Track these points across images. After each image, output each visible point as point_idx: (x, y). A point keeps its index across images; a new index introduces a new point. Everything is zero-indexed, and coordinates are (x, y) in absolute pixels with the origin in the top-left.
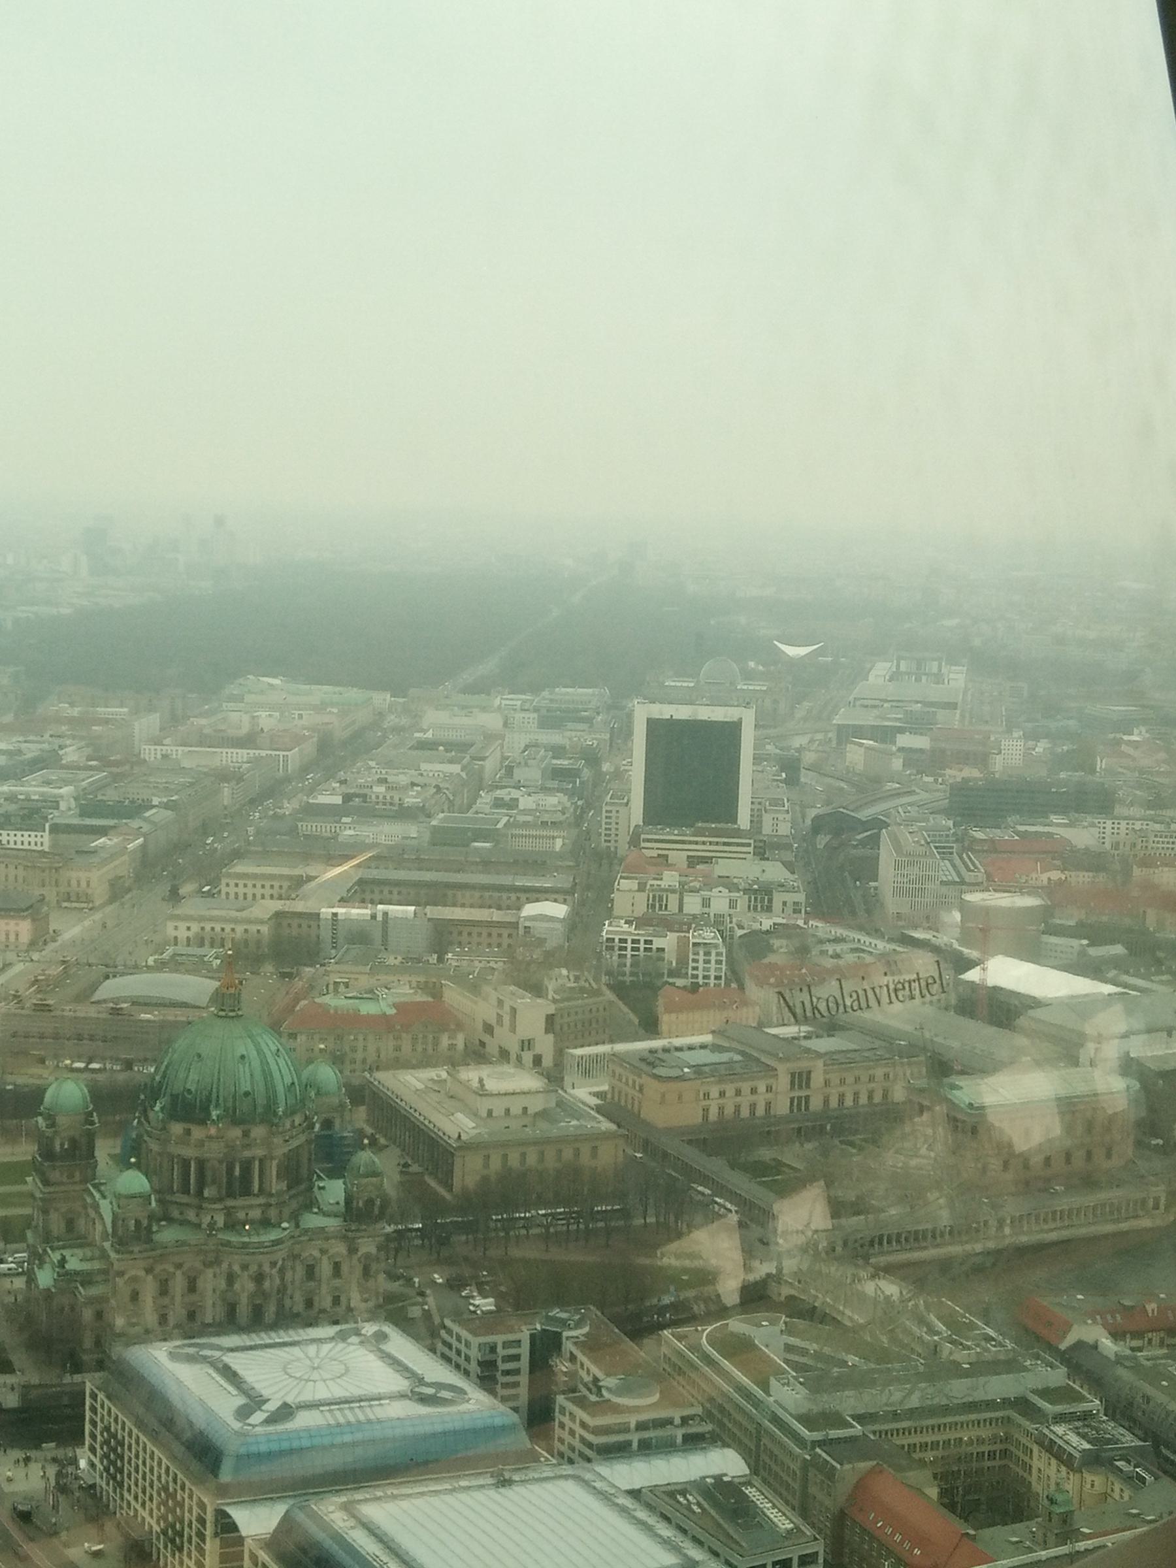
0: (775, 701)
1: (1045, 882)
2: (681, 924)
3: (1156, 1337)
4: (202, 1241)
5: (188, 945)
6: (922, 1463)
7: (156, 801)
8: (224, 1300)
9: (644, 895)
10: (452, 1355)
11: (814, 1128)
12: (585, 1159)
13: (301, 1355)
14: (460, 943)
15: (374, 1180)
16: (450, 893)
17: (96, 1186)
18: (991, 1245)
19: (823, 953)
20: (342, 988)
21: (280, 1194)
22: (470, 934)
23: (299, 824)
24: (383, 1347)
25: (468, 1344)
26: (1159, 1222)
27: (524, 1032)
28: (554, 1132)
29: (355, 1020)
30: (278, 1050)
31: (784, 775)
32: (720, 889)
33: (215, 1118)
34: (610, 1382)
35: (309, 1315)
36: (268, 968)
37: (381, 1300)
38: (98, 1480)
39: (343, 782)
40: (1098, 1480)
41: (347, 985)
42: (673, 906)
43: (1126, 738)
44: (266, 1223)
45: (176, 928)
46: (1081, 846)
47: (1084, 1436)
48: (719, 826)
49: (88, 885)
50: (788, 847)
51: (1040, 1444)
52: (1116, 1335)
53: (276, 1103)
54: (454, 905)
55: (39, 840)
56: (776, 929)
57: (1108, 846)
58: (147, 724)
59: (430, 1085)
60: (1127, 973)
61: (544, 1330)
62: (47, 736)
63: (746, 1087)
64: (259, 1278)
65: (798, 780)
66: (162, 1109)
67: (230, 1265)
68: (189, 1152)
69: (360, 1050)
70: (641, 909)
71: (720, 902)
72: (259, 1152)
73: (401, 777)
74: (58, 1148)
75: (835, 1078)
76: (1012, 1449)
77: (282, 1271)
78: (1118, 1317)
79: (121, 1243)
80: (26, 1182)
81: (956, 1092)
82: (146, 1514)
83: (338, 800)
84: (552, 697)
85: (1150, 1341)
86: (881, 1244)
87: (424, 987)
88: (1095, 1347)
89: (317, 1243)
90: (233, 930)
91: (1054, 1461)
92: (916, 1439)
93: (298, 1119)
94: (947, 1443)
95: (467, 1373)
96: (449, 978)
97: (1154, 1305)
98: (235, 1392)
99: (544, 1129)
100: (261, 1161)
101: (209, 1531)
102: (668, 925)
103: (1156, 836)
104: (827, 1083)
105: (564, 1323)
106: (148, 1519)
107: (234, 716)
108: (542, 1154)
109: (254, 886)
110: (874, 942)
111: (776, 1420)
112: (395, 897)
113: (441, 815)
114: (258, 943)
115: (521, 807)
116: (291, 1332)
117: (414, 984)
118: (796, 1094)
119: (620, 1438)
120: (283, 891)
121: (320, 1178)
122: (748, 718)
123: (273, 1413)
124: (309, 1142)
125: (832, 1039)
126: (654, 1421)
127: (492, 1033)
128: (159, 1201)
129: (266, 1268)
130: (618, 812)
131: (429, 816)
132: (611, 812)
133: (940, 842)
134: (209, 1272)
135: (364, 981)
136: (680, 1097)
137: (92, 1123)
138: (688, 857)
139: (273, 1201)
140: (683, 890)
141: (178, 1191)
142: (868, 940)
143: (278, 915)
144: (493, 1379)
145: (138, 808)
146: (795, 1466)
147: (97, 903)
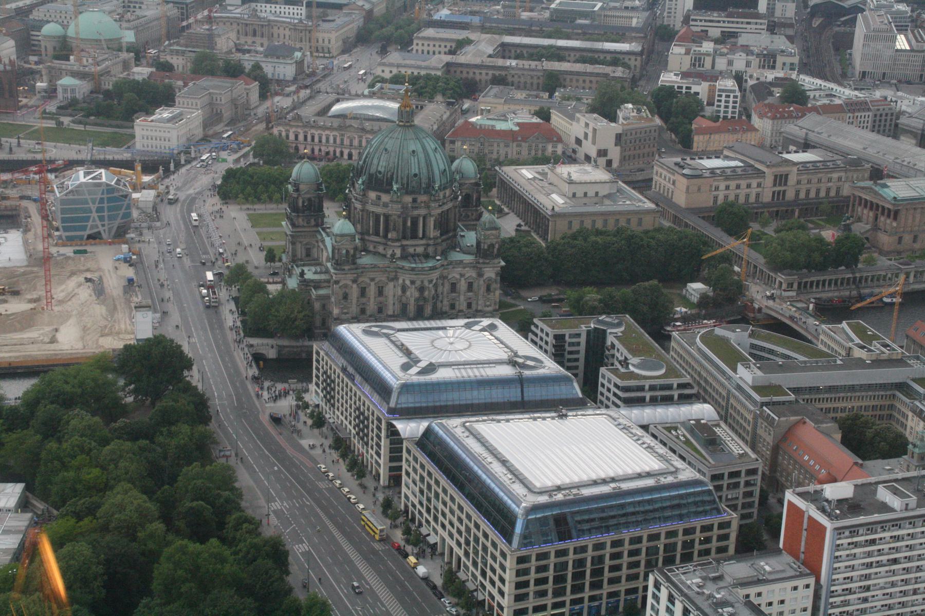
2: (712, 77)
10: (538, 340)
11: (787, 211)
12: (634, 226)
15: (494, 232)
17: (324, 229)
21: (435, 238)
25: (547, 335)
29: (492, 133)
34: (634, 360)
38: (321, 403)
41: (489, 111)
44: (427, 256)
50: (791, 26)
51: (914, 412)
53: (434, 182)
59: (537, 176)
61: (595, 328)
63: (743, 183)
64: (421, 289)
66: (363, 183)
67: (404, 280)
68: (379, 210)
69: (495, 153)
70: (686, 66)
71: (739, 62)
72: (423, 212)
74: (300, 204)
75: (804, 178)
77: (436, 286)
79: (338, 264)
80: (281, 226)
81: (885, 190)
82: (347, 423)
93: (448, 192)
95: (546, 351)
100: (424, 218)
101: (383, 435)
102: (703, 77)
104: (799, 182)
106: (349, 426)
108: (606, 221)
111: (739, 388)
118: (777, 189)
119: (639, 394)
121: (463, 231)
123: (423, 369)
125: (805, 154)
128: (362, 239)
129: (426, 283)
134: (391, 285)
136: (699, 189)
137: (322, 190)
139: (431, 242)
142: (839, 88)
143: (448, 65)
144: (562, 355)
146: (750, 417)
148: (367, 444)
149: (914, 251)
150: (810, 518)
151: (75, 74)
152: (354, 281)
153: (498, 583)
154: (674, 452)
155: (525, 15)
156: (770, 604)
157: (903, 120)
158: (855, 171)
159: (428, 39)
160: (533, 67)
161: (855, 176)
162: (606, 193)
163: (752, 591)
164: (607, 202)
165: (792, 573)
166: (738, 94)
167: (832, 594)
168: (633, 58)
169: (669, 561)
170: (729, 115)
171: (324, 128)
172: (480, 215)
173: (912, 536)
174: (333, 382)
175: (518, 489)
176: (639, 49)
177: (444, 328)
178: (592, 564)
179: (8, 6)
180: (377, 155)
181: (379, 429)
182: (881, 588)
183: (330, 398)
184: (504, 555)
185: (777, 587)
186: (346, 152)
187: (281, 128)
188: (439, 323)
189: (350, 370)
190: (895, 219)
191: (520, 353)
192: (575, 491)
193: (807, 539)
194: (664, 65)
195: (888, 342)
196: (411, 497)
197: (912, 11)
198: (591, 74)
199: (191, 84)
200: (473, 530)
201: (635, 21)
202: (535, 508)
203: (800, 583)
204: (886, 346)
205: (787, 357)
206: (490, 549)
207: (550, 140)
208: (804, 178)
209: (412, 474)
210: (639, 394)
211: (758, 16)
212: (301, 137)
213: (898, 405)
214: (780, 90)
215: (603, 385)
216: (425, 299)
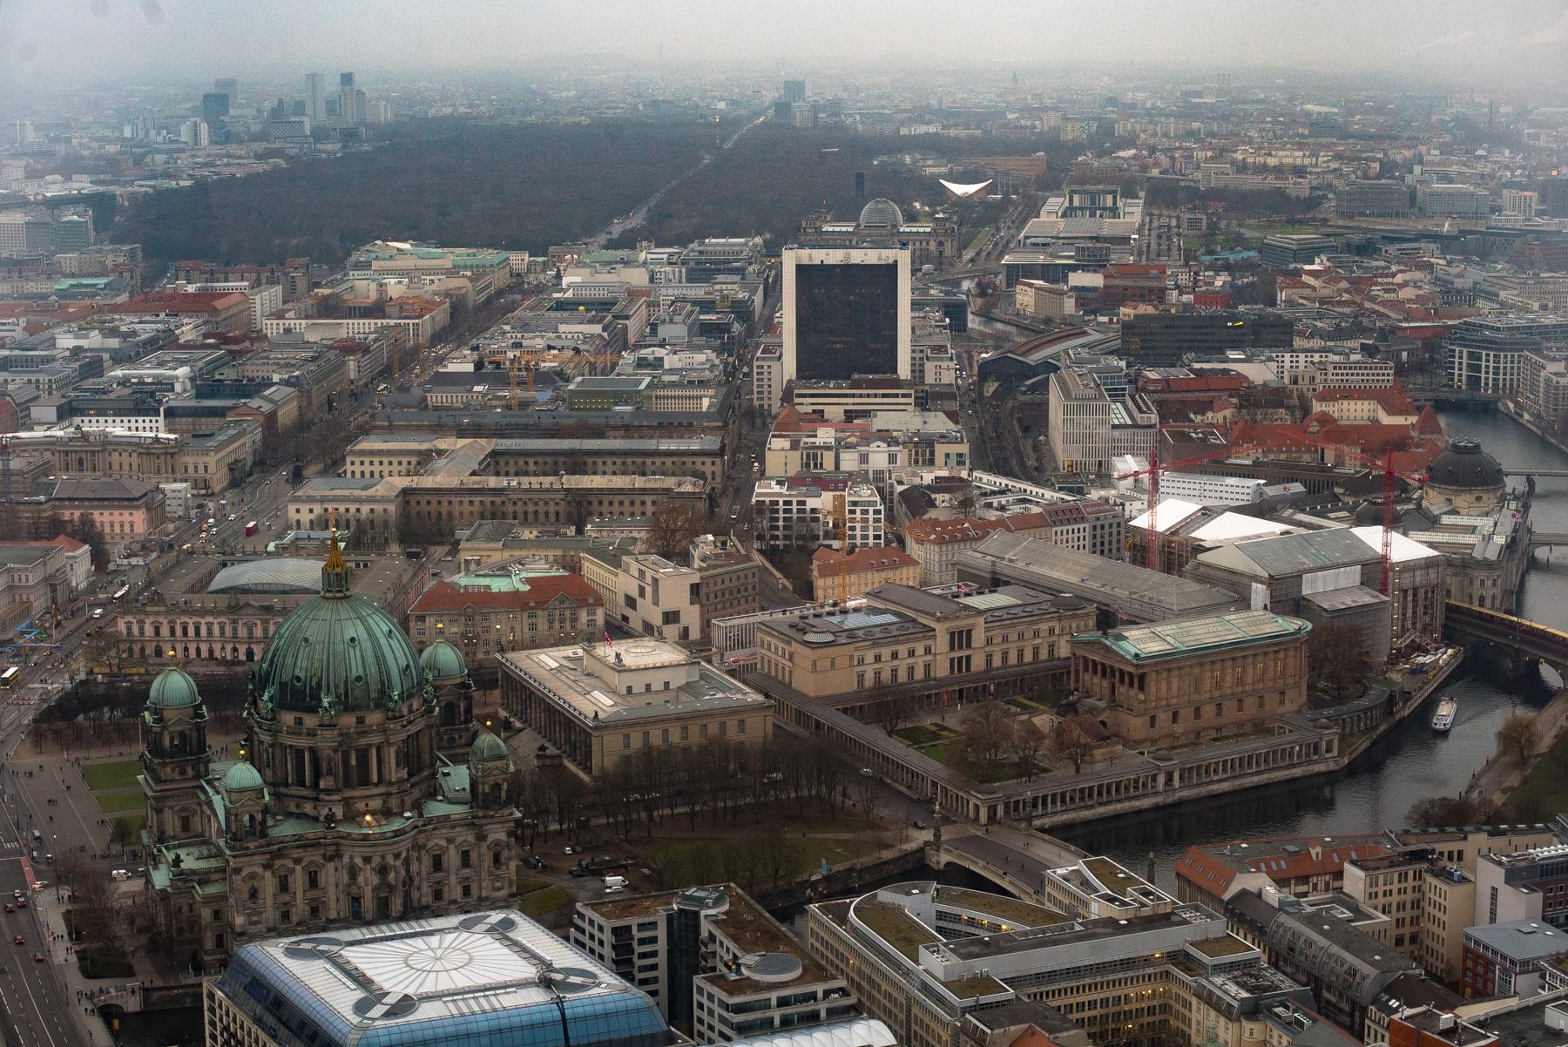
0: (941, 244)
1: (1221, 421)
2: (836, 482)
3: (1321, 881)
4: (321, 834)
5: (312, 528)
6: (1080, 1023)
7: (276, 378)
8: (349, 894)
9: (798, 453)
10: (586, 940)
11: (976, 689)
12: (733, 734)
13: (424, 946)
14: (601, 514)
15: (499, 763)
16: (590, 460)
17: (209, 782)
18: (1160, 799)
19: (990, 505)
20: (473, 567)
21: (400, 782)
22: (611, 503)
23: (429, 395)
24: (511, 935)
25: (601, 928)
26: (1332, 766)
27: (668, 604)
29: (488, 600)
30: (390, 631)
31: (948, 320)
32: (879, 443)
33: (326, 704)
34: (749, 959)
36: (395, 548)
37: (514, 889)
39: (475, 348)
40: (1256, 1027)
41: (478, 563)
43: (1307, 267)
44: (386, 813)
45: (298, 511)
48: (877, 377)
49: (206, 471)
50: (952, 396)
51: (1199, 997)
52: (1281, 882)
53: (391, 688)
54: (595, 473)
55: (154, 425)
56: (941, 485)
57: (1286, 380)
58: (267, 298)
59: (565, 663)
60: (1303, 511)
62: (162, 315)
63: (903, 650)
64: (383, 870)
65: (966, 324)
66: (271, 699)
67: (351, 858)
68: (302, 742)
70: (794, 467)
71: (879, 457)
72: (375, 739)
73: (538, 340)
74: (167, 743)
75: (997, 635)
76: (1173, 1003)
77: (407, 863)
78: (1283, 863)
83: (470, 368)
84: (701, 248)
85: (1315, 886)
86: (1044, 804)
88: (1259, 895)
89: (445, 831)
90: (358, 510)
91: (1213, 1013)
92: (1073, 1000)
94: (1105, 1002)
95: (601, 957)
97: (1319, 849)
98: (353, 987)
99: (687, 704)
100: (379, 749)
103: (1335, 368)
104: (989, 641)
105: (700, 902)
107: (361, 285)
109: (381, 463)
110: (1041, 491)
111: (925, 988)
112: (532, 467)
113: (579, 379)
114: (386, 522)
115: (667, 366)
116: (423, 922)
117: (551, 559)
118: (957, 654)
120: (412, 467)
122: (904, 259)
123: (393, 1006)
124: (430, 727)
126: (796, 996)
127: (634, 608)
129: (390, 860)
130: (769, 367)
131: (568, 380)
132: (762, 367)
133: (1112, 384)
134: (331, 866)
135: (497, 557)
137: (202, 716)
138: (846, 411)
139: (394, 789)
140: (840, 446)
141: (293, 784)
142: (1035, 490)
143: (405, 492)
144: (630, 962)
145: (256, 387)
147: (217, 490)
149: (1173, 736)
152: (266, 867)
158: (1074, 617)
159: (372, 453)
160: (546, 485)
161: (1074, 626)
168: (708, 460)
170: (871, 541)
171: (203, 612)
172: (475, 735)
177: (431, 933)
180: (292, 649)
187: (129, 618)
188: (416, 927)
190: (1141, 688)
191: (557, 965)
198: (643, 491)
204: (1146, 894)
207: (583, 603)
212: (165, 631)
215: (701, 1006)
216: (389, 886)
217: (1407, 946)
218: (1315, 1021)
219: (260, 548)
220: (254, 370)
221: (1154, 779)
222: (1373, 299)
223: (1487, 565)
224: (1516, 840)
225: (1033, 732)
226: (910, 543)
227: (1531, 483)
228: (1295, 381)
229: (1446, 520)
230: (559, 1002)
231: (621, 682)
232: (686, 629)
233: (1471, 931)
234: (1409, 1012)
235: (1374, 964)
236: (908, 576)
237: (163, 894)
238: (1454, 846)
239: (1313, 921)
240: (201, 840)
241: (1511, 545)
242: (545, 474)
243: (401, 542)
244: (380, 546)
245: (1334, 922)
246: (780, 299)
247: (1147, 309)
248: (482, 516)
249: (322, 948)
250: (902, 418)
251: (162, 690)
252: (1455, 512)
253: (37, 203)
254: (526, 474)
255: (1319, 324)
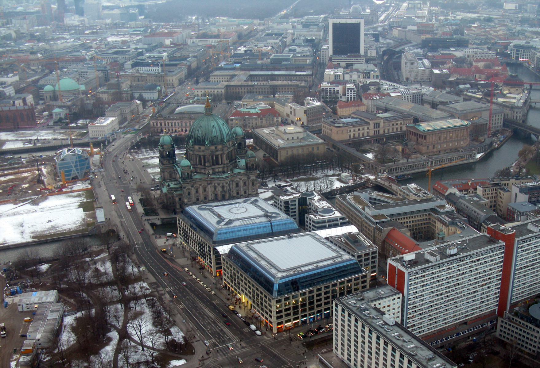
0: (372, 17)
2: (344, 83)
7: (191, 55)
10: (277, 205)
12: (315, 151)
15: (253, 159)
17: (176, 164)
21: (227, 164)
24: (257, 204)
28: (306, 143)
35: (238, 196)
36: (224, 101)
41: (247, 105)
42: (341, 78)
44: (224, 172)
46: (458, 57)
47: (449, 218)
50: (375, 60)
51: (438, 220)
52: (460, 191)
53: (224, 138)
56: (373, 84)
63: (361, 128)
64: (223, 187)
68: (200, 154)
71: (355, 76)
72: (220, 152)
74: (165, 154)
75: (386, 124)
77: (229, 185)
79: (184, 179)
87: (270, 105)
88: (455, 194)
91: (441, 225)
94: (413, 221)
95: (281, 209)
96: (276, 102)
97: (470, 182)
100: (221, 155)
101: (212, 253)
102: (340, 83)
104: (384, 126)
111: (366, 217)
112: (261, 79)
114: (221, 95)
115: (297, 51)
118: (376, 129)
119: (323, 224)
122: (362, 22)
124: (234, 149)
128: (194, 168)
129: (225, 184)
134: (209, 186)
139: (225, 166)
142: (397, 85)
143: (227, 87)
144: (288, 211)
145: (185, 58)
146: (372, 229)
148: (205, 258)
149: (433, 152)
150: (398, 269)
151: (60, 107)
152: (192, 186)
153: (269, 313)
154: (340, 248)
155: (259, 62)
156: (384, 307)
157: (424, 97)
159: (217, 76)
160: (265, 84)
162: (302, 137)
163: (376, 303)
164: (302, 141)
165: (393, 293)
166: (356, 90)
167: (409, 300)
168: (309, 77)
169: (342, 294)
170: (353, 99)
171: (173, 119)
172: (247, 151)
173: (439, 272)
174: (187, 232)
175: (273, 271)
176: (311, 73)
177: (236, 203)
178: (309, 300)
179: (28, 80)
181: (210, 251)
182: (429, 295)
183: (186, 239)
184: (270, 300)
185: (387, 300)
186: (184, 129)
187: (154, 121)
188: (232, 202)
189: (194, 226)
191: (269, 211)
192: (298, 269)
193: (398, 278)
194: (322, 79)
195: (426, 192)
196: (227, 280)
197: (423, 52)
198: (291, 85)
199: (112, 106)
200: (256, 291)
201: (308, 61)
202: (282, 278)
203: (396, 297)
204: (425, 193)
205: (386, 202)
206: (264, 298)
207: (275, 116)
208: (386, 124)
209: (227, 269)
210: (323, 224)
211: (360, 56)
212: (163, 124)
213: (432, 218)
214: (373, 87)
215: (307, 222)
217: (493, 208)
218: (468, 227)
219: (188, 102)
220: (185, 53)
221: (428, 163)
222: (491, 34)
223: (518, 108)
224: (522, 181)
225: (396, 151)
226: (363, 99)
227: (531, 86)
228: (469, 56)
229: (508, 95)
230: (270, 221)
231: (286, 137)
232: (303, 123)
233: (509, 204)
234: (492, 225)
235: (485, 213)
236: (363, 109)
237: (166, 194)
238: (506, 182)
239: (469, 201)
240: (175, 180)
241: (525, 103)
242: (264, 81)
243: (226, 99)
244: (220, 100)
245: (474, 201)
246: (328, 33)
247: (428, 36)
248: (248, 93)
249: (208, 207)
250: (361, 66)
251: (163, 141)
252: (510, 93)
253: (123, 8)
254: (259, 81)
255: (476, 41)
